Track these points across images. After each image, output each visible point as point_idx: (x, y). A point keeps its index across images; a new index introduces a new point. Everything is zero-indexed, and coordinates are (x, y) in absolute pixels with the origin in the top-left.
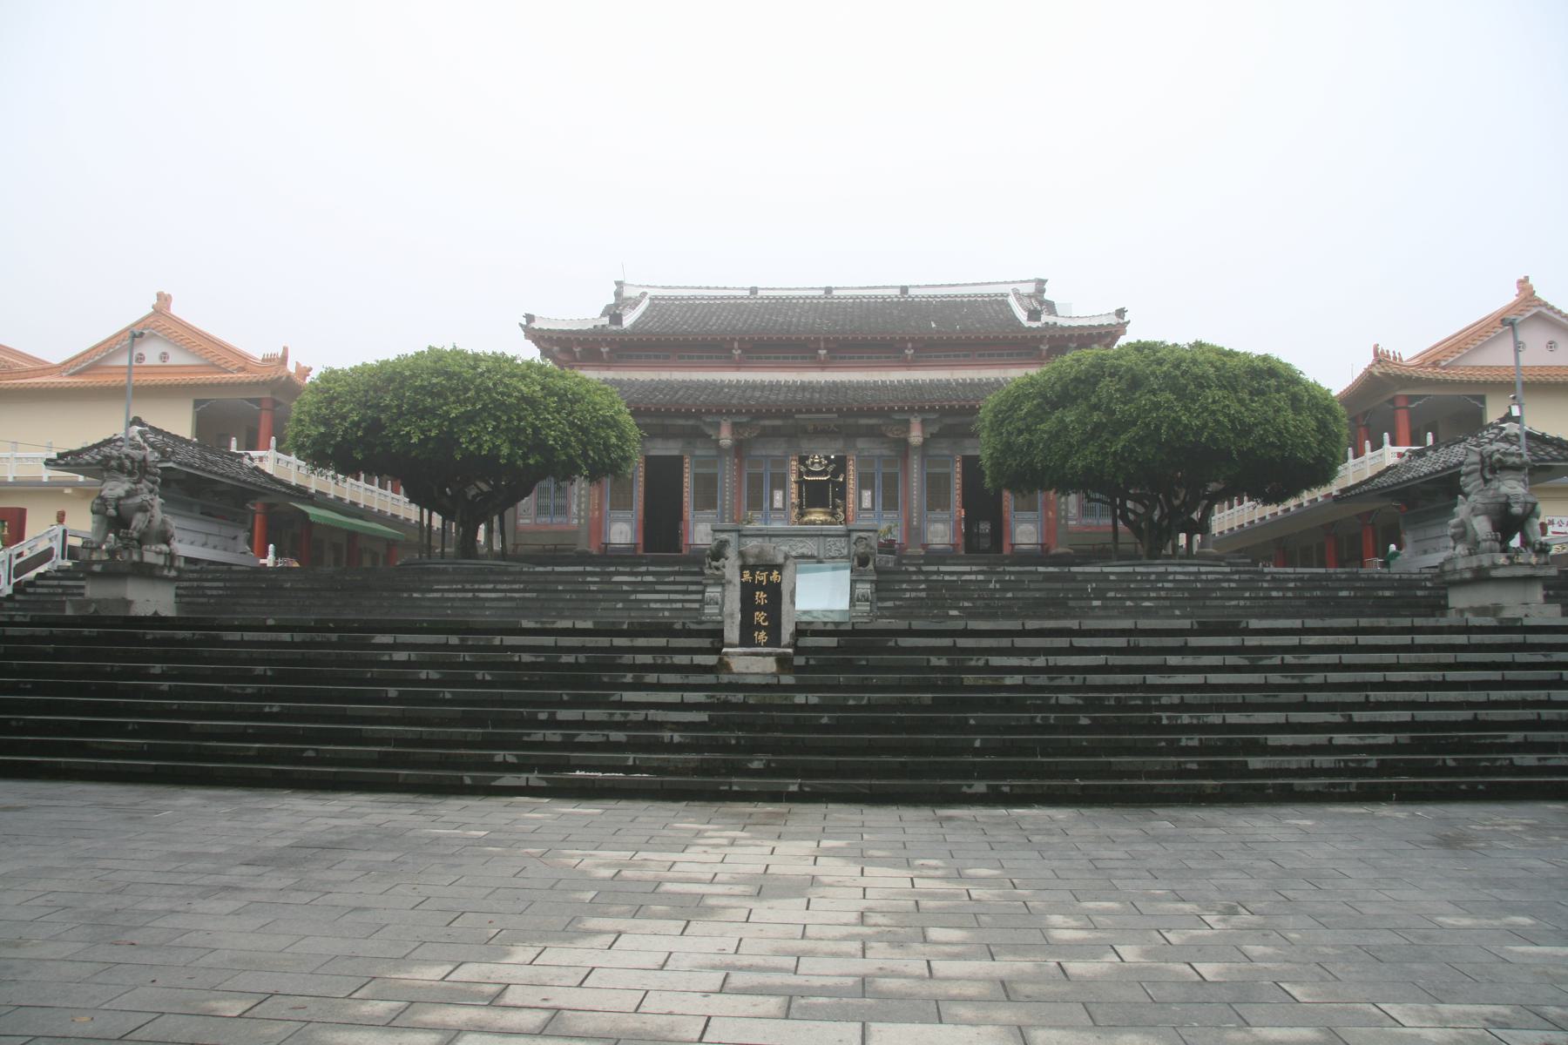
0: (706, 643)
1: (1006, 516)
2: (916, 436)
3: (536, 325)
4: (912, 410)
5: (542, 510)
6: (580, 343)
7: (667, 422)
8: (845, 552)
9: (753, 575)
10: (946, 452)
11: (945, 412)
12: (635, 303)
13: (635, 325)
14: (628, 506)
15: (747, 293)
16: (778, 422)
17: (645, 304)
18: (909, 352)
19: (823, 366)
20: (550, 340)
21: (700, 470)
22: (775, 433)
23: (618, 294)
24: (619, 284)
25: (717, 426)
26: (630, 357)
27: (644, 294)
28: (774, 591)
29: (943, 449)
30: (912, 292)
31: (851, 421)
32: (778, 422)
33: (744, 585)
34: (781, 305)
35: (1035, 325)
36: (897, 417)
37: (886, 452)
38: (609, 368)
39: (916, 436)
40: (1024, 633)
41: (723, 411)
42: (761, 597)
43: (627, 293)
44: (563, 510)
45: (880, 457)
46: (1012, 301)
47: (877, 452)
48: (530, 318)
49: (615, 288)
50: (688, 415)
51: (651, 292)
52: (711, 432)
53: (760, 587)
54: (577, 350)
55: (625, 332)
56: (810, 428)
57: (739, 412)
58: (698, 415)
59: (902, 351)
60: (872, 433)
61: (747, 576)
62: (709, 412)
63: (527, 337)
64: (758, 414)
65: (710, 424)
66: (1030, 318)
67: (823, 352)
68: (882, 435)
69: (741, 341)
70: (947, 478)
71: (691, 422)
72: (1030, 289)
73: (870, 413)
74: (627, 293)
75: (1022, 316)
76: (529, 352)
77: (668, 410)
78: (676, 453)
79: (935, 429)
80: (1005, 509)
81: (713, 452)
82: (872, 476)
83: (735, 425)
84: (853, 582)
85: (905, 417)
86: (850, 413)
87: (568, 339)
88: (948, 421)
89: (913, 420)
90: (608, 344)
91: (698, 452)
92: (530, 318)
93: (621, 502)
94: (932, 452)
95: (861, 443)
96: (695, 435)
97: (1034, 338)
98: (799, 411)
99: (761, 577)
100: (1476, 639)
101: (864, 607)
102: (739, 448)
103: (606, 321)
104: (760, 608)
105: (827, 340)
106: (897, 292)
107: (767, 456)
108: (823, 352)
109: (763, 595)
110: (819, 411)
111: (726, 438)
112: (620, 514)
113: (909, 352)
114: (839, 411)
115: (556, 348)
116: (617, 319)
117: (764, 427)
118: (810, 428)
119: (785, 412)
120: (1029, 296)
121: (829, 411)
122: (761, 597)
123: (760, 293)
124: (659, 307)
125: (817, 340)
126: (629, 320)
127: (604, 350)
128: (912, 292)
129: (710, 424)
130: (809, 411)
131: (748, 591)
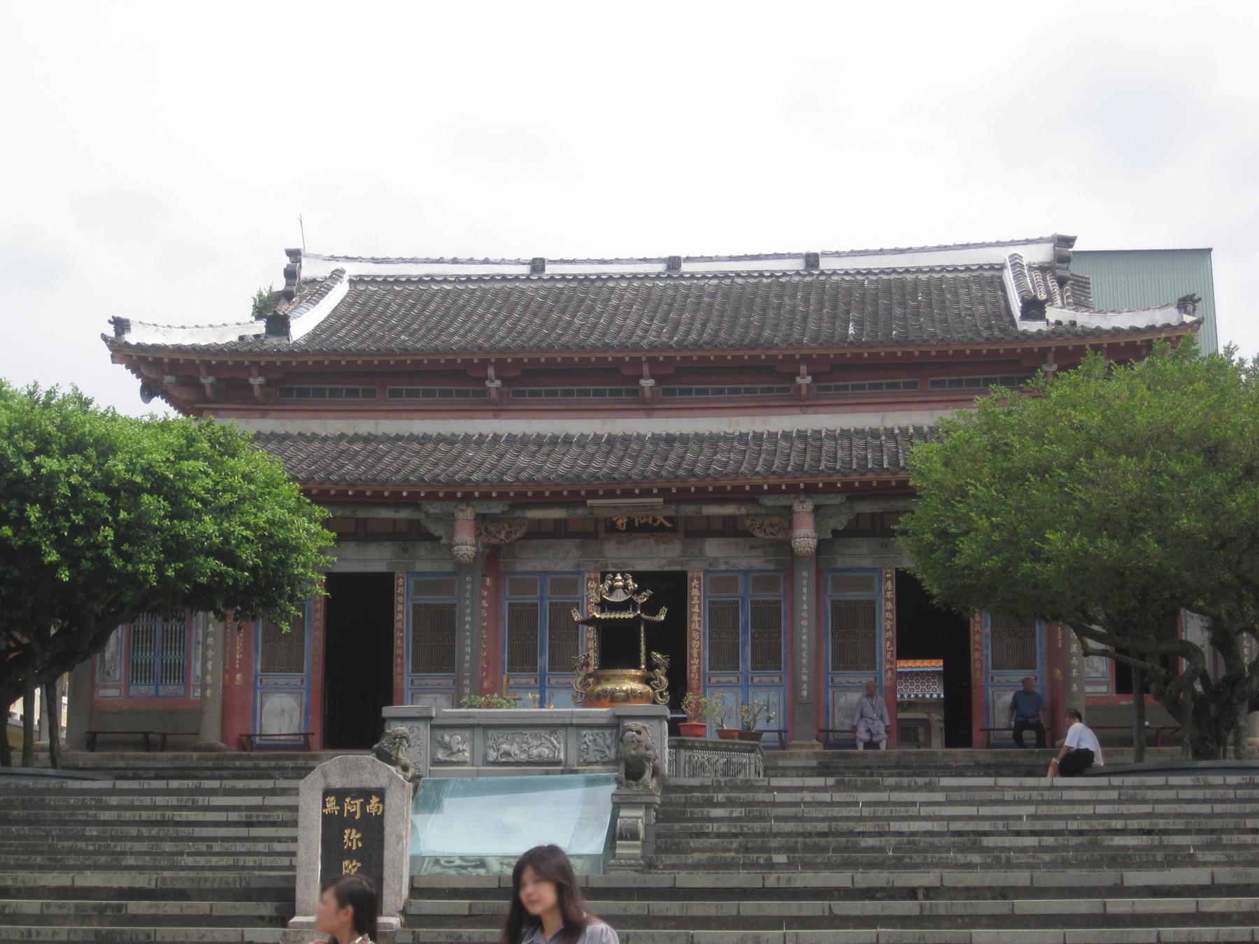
0: (267, 909)
1: (976, 676)
2: (805, 537)
3: (132, 338)
4: (793, 490)
5: (137, 672)
6: (211, 370)
7: (362, 514)
8: (611, 754)
9: (340, 802)
10: (868, 563)
11: (856, 493)
12: (318, 289)
13: (313, 336)
14: (294, 665)
15: (524, 270)
16: (558, 513)
17: (340, 291)
18: (805, 381)
19: (648, 408)
20: (158, 362)
21: (425, 599)
22: (559, 531)
23: (291, 274)
24: (294, 255)
25: (449, 521)
26: (303, 393)
27: (337, 275)
28: (373, 829)
29: (859, 555)
30: (825, 264)
31: (689, 510)
32: (558, 513)
33: (327, 819)
34: (587, 291)
35: (1033, 326)
36: (770, 501)
37: (758, 564)
38: (264, 413)
39: (805, 537)
40: (1119, 891)
41: (458, 494)
42: (352, 837)
43: (308, 271)
44: (178, 672)
45: (746, 572)
46: (1008, 276)
47: (743, 564)
48: (121, 325)
49: (287, 261)
50: (396, 501)
51: (352, 270)
52: (437, 529)
53: (350, 822)
54: (208, 381)
55: (299, 352)
56: (621, 522)
57: (485, 497)
58: (413, 501)
59: (791, 378)
60: (730, 529)
61: (332, 806)
62: (432, 497)
63: (115, 359)
64: (524, 497)
65: (438, 518)
66: (1026, 315)
67: (647, 383)
68: (746, 534)
69: (500, 365)
70: (870, 609)
71: (404, 514)
72: (1042, 254)
73: (721, 496)
74: (308, 271)
75: (1016, 306)
76: (120, 395)
77: (360, 494)
78: (380, 567)
79: (840, 522)
80: (975, 666)
81: (448, 567)
82: (733, 609)
83: (481, 518)
84: (616, 807)
85: (449, 507)
86: (683, 496)
87: (190, 363)
88: (866, 508)
89: (797, 507)
90: (262, 371)
91: (420, 567)
92: (121, 325)
93: (282, 657)
94: (842, 562)
95: (714, 548)
96: (411, 536)
97: (1028, 352)
98: (593, 494)
99: (353, 807)
100: (729, 907)
101: (629, 850)
102: (492, 559)
103: (260, 327)
104: (350, 855)
105: (652, 361)
106: (798, 265)
107: (544, 573)
108: (647, 383)
109: (355, 835)
110: (628, 493)
111: (466, 544)
112: (281, 679)
113: (805, 381)
114: (663, 492)
115: (169, 379)
116: (279, 325)
117: (533, 522)
118: (621, 522)
119: (570, 494)
120: (1043, 269)
121: (646, 493)
122: (352, 837)
123: (550, 270)
124: (373, 296)
125: (636, 362)
126: (303, 324)
127: (256, 381)
128: (825, 264)
129: (438, 518)
130: (610, 494)
131: (333, 826)
